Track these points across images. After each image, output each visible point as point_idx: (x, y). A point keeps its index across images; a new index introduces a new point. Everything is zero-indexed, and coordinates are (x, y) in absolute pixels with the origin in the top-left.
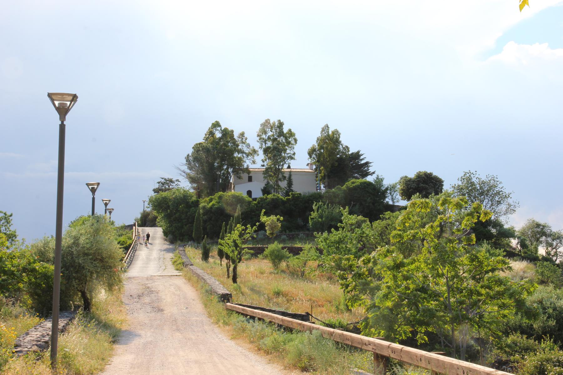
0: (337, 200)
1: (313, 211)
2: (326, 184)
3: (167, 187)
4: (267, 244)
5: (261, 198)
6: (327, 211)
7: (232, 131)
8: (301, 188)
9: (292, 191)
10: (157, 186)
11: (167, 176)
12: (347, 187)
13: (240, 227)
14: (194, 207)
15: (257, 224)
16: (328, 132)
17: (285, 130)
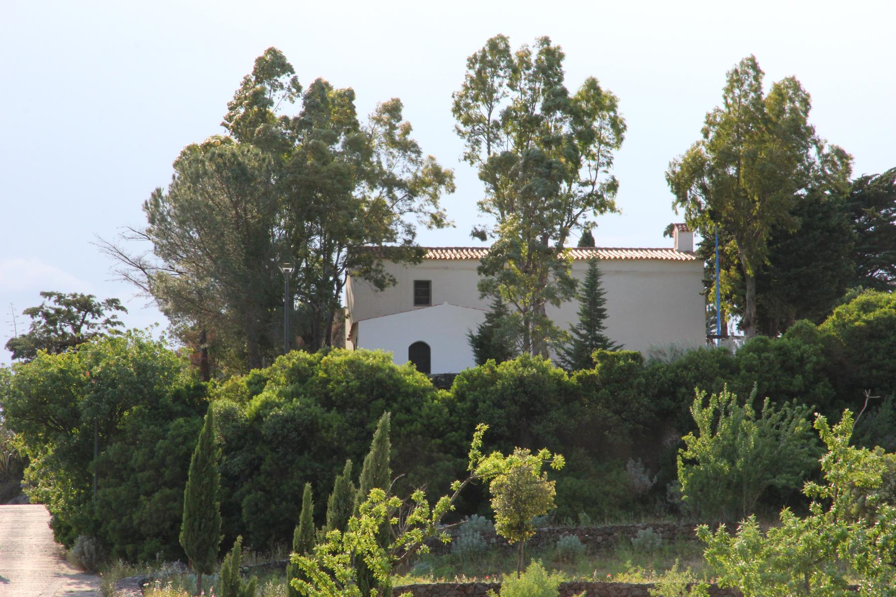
0: (798, 380)
1: (693, 427)
2: (751, 310)
3: (69, 329)
4: (497, 574)
5: (469, 377)
6: (755, 429)
7: (349, 95)
8: (641, 331)
9: (603, 343)
10: (24, 327)
11: (72, 286)
12: (842, 326)
13: (378, 502)
14: (184, 414)
15: (456, 485)
16: (757, 89)
17: (573, 85)
